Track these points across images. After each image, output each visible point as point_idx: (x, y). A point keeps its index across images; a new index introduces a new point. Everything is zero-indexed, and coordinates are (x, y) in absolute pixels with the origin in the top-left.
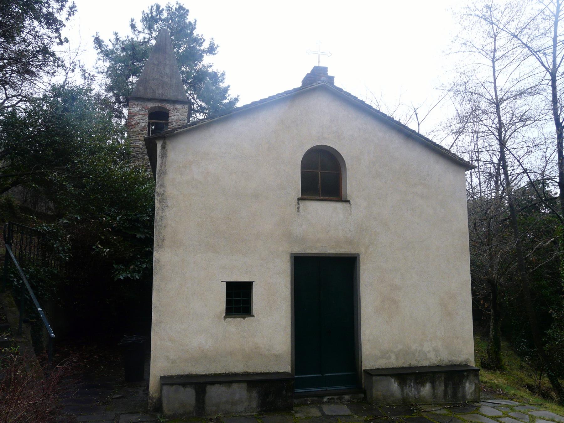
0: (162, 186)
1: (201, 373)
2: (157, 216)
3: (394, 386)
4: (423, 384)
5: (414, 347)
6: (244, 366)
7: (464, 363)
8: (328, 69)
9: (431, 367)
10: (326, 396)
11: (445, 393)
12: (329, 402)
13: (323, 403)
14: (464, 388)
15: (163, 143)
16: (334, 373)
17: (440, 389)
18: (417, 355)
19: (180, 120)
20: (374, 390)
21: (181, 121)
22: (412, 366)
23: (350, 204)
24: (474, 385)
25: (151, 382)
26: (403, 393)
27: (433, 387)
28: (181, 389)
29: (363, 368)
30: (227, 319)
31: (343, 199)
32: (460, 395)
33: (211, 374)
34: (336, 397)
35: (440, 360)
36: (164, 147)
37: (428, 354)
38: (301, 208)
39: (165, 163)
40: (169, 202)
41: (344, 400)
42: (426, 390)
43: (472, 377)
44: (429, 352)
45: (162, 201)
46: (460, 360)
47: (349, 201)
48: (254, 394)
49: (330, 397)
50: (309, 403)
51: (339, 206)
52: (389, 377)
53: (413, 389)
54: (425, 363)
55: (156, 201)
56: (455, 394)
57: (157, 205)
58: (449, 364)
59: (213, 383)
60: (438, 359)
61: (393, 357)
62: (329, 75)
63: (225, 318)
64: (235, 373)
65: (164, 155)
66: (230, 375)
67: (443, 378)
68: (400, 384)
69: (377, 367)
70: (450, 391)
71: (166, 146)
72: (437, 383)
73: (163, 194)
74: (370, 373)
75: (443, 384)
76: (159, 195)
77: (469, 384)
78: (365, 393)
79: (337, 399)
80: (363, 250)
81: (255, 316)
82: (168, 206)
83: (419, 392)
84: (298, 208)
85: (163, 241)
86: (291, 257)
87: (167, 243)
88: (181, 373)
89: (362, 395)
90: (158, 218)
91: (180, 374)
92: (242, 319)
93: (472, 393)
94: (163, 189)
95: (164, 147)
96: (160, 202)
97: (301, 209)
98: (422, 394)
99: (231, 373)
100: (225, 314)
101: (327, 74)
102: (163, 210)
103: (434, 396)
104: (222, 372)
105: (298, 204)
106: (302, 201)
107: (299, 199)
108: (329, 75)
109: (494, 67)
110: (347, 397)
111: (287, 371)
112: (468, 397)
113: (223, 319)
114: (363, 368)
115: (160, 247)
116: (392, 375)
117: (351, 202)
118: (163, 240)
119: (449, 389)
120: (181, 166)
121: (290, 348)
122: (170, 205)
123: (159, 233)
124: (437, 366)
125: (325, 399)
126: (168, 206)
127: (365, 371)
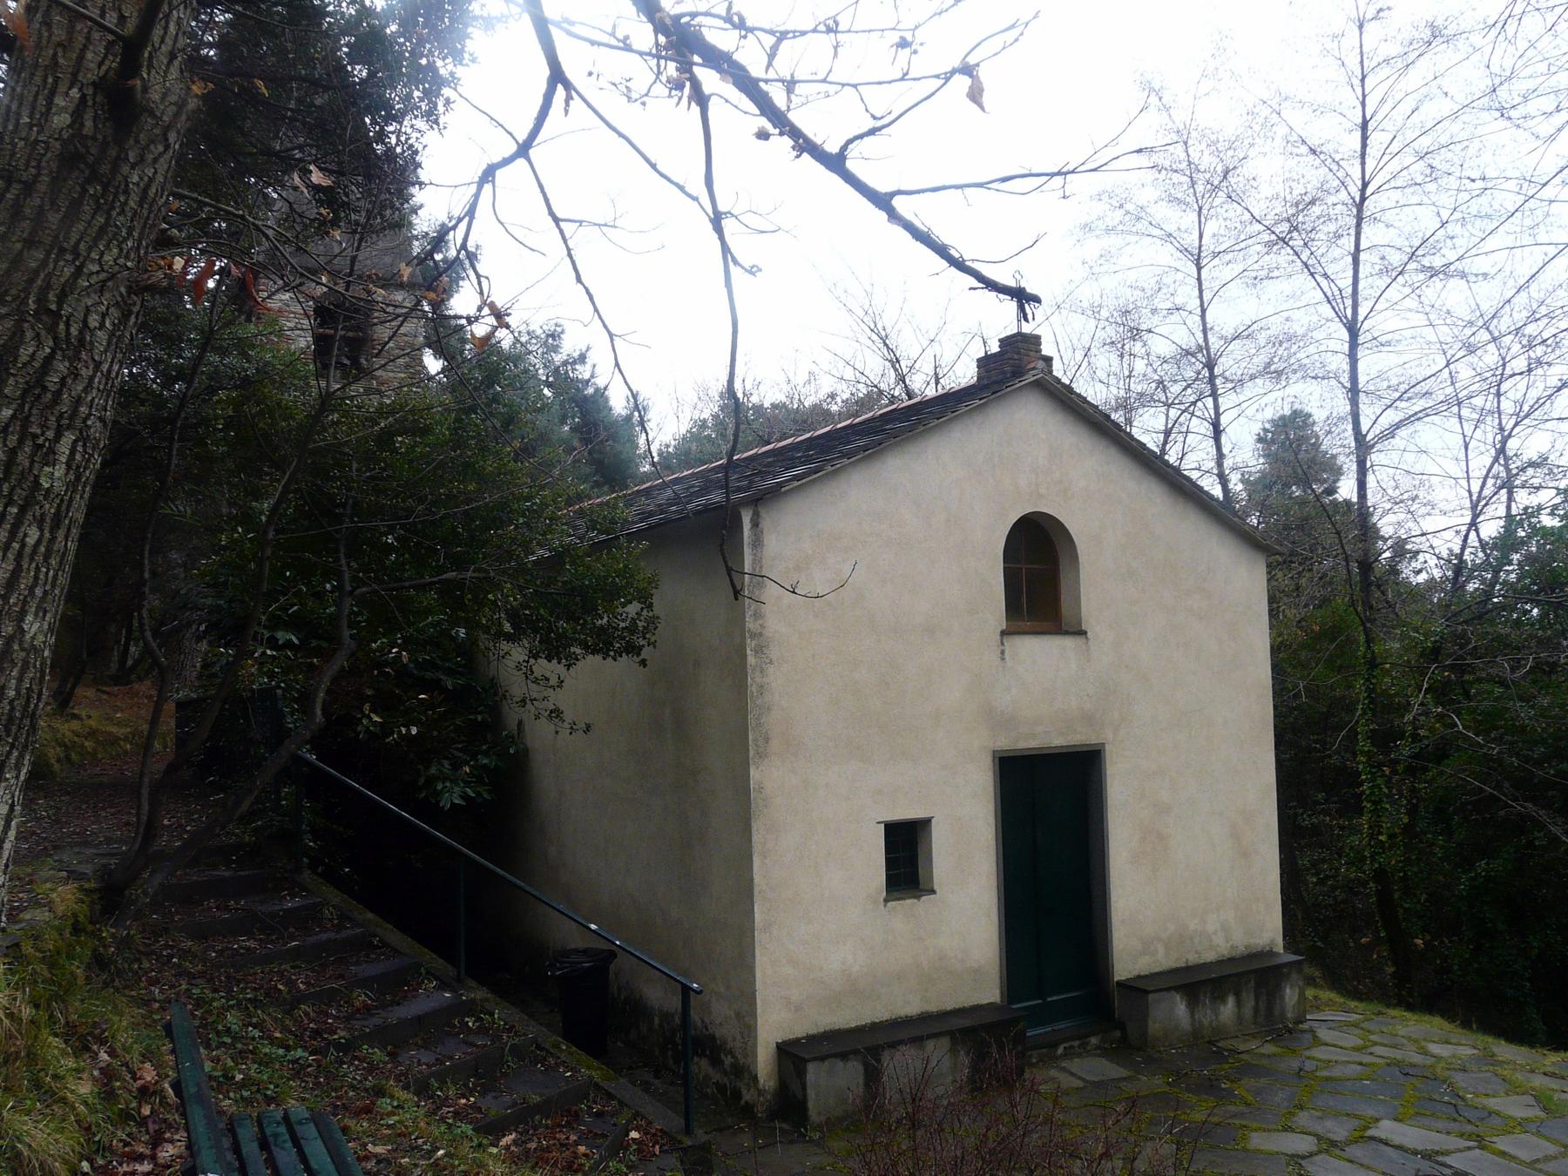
0: (758, 615)
1: (847, 1026)
2: (751, 685)
3: (1180, 1008)
4: (1221, 998)
5: (1192, 926)
6: (921, 1000)
7: (1268, 949)
8: (1042, 340)
9: (1220, 963)
10: (1060, 1044)
11: (1256, 1010)
12: (1066, 1055)
13: (1057, 1058)
14: (1282, 998)
15: (754, 514)
16: (1062, 994)
17: (1249, 1004)
18: (1196, 941)
19: (406, 335)
20: (1150, 1023)
21: (406, 339)
22: (1190, 964)
23: (1087, 638)
24: (1297, 990)
25: (759, 1058)
26: (1194, 1020)
27: (1239, 1003)
28: (840, 1064)
29: (1116, 979)
30: (889, 904)
31: (1064, 628)
32: (1276, 1013)
33: (865, 1026)
34: (1076, 1043)
35: (1232, 947)
36: (755, 524)
37: (1213, 937)
38: (1007, 652)
39: (760, 561)
40: (774, 652)
41: (1089, 1048)
42: (1228, 1009)
43: (1294, 976)
44: (1215, 933)
45: (759, 650)
46: (1261, 942)
47: (1083, 633)
48: (964, 1059)
49: (1065, 1045)
50: (1034, 1061)
51: (1068, 643)
52: (1173, 992)
53: (1209, 1011)
54: (1210, 957)
55: (748, 652)
56: (1270, 1009)
57: (751, 660)
58: (1246, 953)
59: (893, 1045)
60: (1229, 945)
61: (1161, 950)
62: (1043, 353)
63: (886, 901)
64: (907, 1017)
65: (757, 543)
66: (898, 1023)
67: (1252, 984)
68: (1189, 1004)
69: (1136, 973)
70: (1262, 1005)
71: (760, 520)
72: (1244, 994)
73: (761, 634)
74: (1139, 988)
75: (1252, 996)
76: (753, 636)
77: (1291, 988)
78: (1123, 1028)
79: (1079, 1047)
80: (1110, 736)
81: (938, 891)
82: (771, 662)
83: (1217, 1015)
84: (1003, 652)
85: (767, 742)
86: (994, 757)
87: (775, 744)
88: (813, 1031)
89: (1118, 1034)
90: (754, 689)
91: (811, 1032)
92: (916, 901)
93: (1294, 1005)
94: (760, 622)
95: (755, 524)
96: (756, 652)
97: (1007, 655)
98: (1222, 1017)
99: (900, 1018)
100: (885, 893)
101: (1041, 351)
102: (762, 671)
103: (1240, 1019)
104: (885, 1019)
105: (1002, 644)
106: (1011, 637)
107: (1003, 633)
108: (1043, 353)
109: (1199, 279)
110: (1094, 1040)
111: (992, 1000)
112: (1289, 1015)
113: (882, 903)
114: (1116, 979)
115: (762, 756)
116: (1177, 989)
117: (1089, 634)
118: (767, 740)
119: (1260, 1003)
120: (791, 566)
121: (997, 952)
122: (774, 658)
123: (759, 725)
124: (1229, 959)
125: (1060, 1051)
126: (771, 662)
127: (1118, 983)
